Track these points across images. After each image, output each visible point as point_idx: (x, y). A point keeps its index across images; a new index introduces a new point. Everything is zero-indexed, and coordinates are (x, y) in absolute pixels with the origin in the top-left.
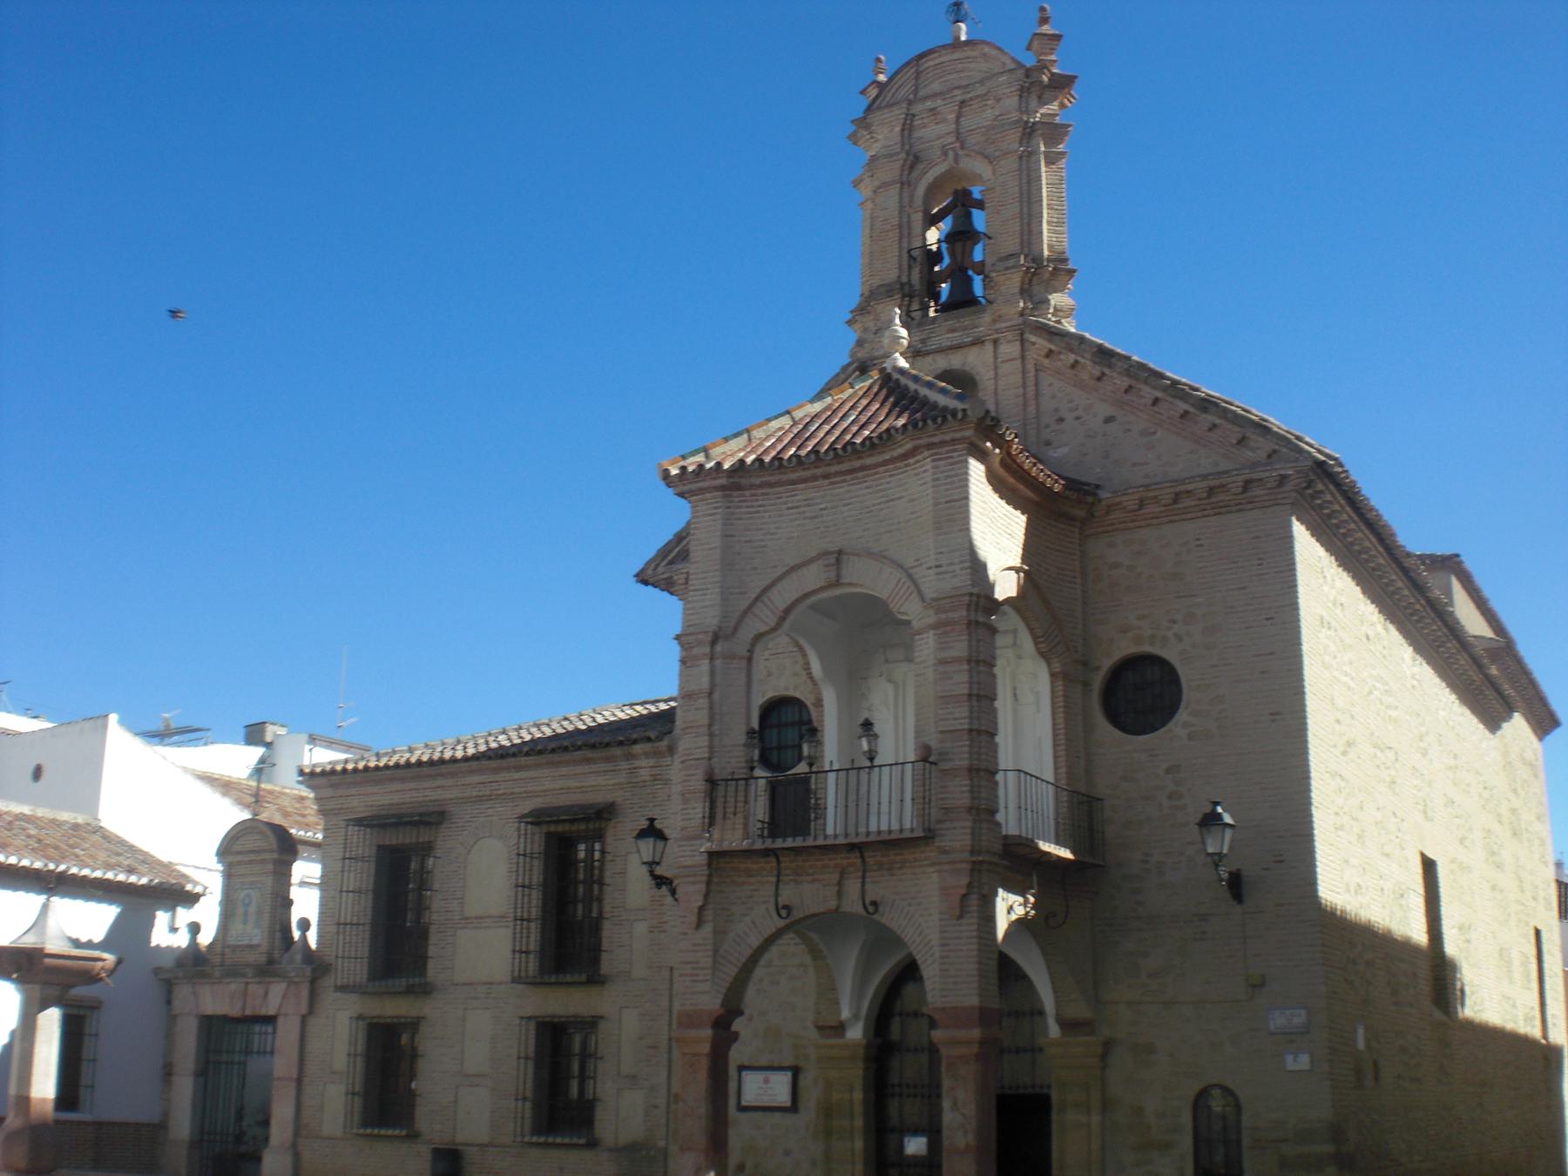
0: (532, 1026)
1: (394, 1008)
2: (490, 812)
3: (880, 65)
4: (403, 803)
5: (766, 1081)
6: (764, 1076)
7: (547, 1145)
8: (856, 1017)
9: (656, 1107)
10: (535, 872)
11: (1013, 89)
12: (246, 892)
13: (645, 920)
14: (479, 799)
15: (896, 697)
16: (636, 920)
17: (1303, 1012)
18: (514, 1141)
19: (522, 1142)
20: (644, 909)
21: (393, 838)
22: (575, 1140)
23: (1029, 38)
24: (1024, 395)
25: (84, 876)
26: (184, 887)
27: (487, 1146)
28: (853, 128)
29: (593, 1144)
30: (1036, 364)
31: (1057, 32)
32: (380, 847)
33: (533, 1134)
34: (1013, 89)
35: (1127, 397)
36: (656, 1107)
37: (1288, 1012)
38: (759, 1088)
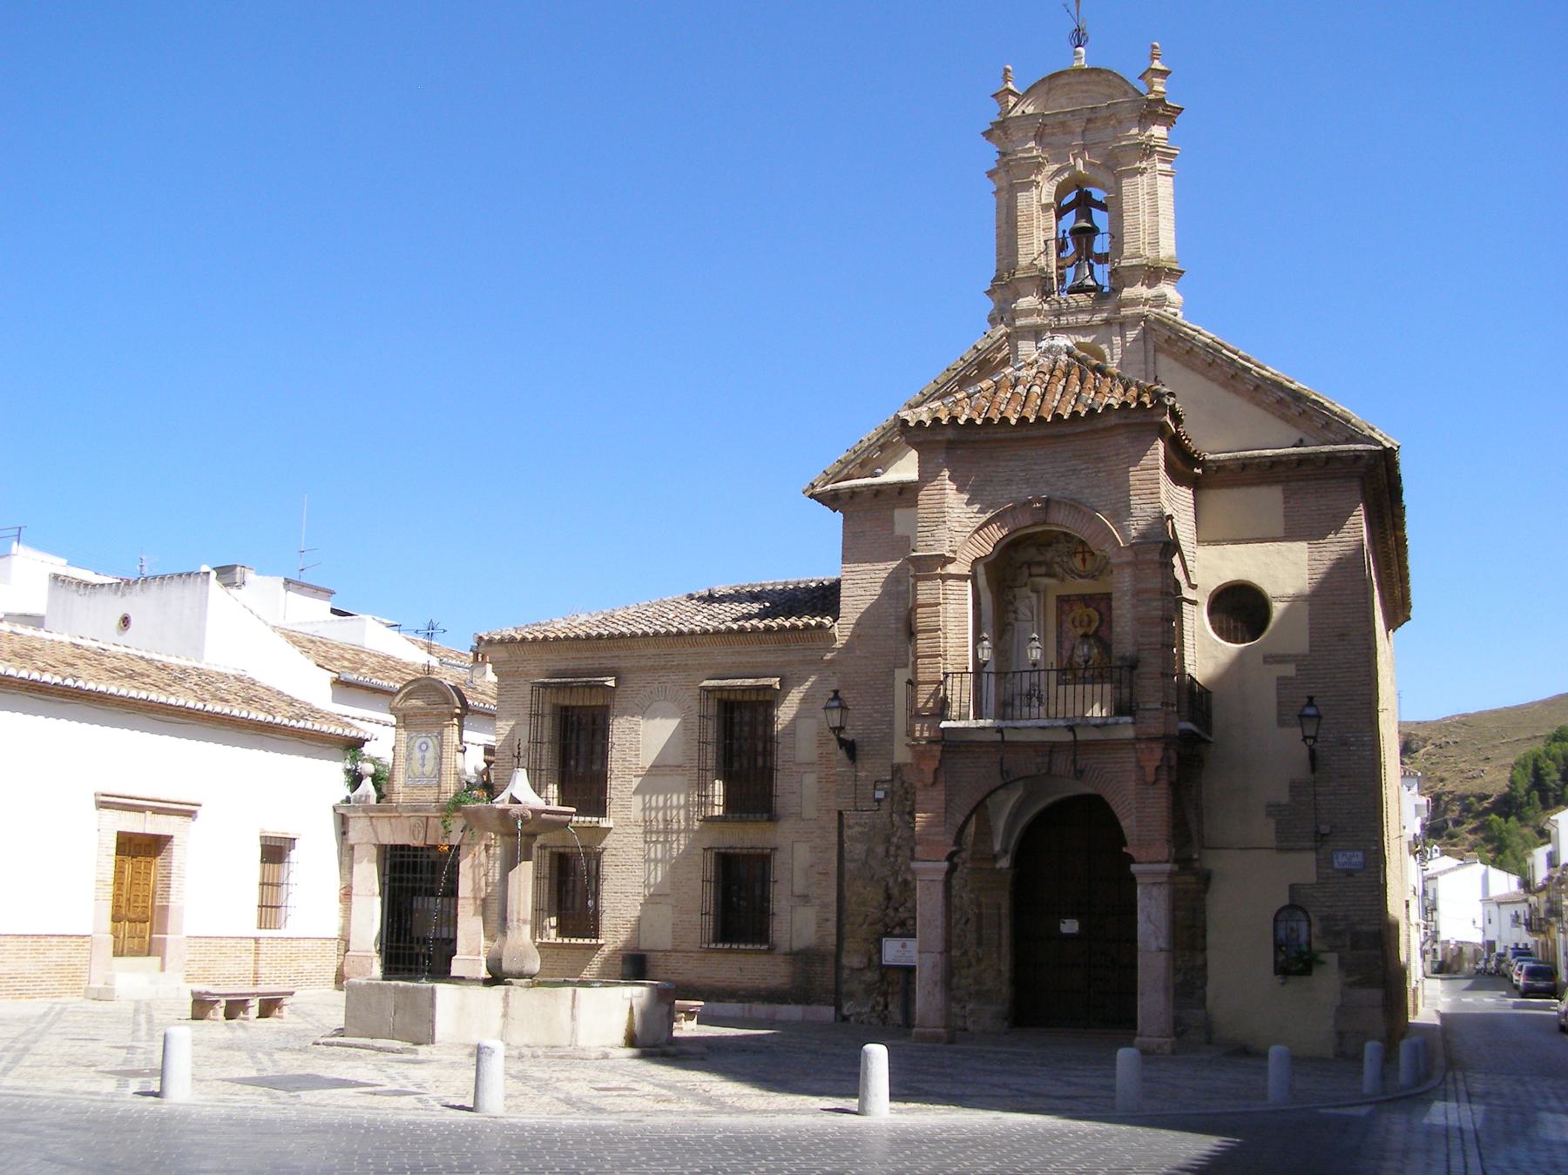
0: (711, 856)
1: (746, 837)
2: (663, 679)
3: (1009, 74)
4: (579, 669)
5: (904, 946)
6: (901, 942)
7: (730, 951)
8: (1005, 851)
9: (827, 920)
10: (710, 731)
11: (1135, 115)
12: (424, 739)
13: (814, 772)
14: (653, 669)
15: (1039, 602)
16: (805, 772)
17: (1360, 854)
18: (701, 947)
19: (708, 948)
20: (813, 764)
21: (566, 700)
22: (757, 946)
23: (1145, 70)
24: (1146, 369)
25: (292, 726)
26: (1180, 868)
27: (670, 951)
28: (990, 127)
29: (771, 950)
30: (1155, 346)
31: (1166, 69)
32: (555, 706)
33: (715, 941)
34: (1135, 115)
35: (1232, 382)
36: (827, 920)
37: (1348, 854)
38: (898, 951)
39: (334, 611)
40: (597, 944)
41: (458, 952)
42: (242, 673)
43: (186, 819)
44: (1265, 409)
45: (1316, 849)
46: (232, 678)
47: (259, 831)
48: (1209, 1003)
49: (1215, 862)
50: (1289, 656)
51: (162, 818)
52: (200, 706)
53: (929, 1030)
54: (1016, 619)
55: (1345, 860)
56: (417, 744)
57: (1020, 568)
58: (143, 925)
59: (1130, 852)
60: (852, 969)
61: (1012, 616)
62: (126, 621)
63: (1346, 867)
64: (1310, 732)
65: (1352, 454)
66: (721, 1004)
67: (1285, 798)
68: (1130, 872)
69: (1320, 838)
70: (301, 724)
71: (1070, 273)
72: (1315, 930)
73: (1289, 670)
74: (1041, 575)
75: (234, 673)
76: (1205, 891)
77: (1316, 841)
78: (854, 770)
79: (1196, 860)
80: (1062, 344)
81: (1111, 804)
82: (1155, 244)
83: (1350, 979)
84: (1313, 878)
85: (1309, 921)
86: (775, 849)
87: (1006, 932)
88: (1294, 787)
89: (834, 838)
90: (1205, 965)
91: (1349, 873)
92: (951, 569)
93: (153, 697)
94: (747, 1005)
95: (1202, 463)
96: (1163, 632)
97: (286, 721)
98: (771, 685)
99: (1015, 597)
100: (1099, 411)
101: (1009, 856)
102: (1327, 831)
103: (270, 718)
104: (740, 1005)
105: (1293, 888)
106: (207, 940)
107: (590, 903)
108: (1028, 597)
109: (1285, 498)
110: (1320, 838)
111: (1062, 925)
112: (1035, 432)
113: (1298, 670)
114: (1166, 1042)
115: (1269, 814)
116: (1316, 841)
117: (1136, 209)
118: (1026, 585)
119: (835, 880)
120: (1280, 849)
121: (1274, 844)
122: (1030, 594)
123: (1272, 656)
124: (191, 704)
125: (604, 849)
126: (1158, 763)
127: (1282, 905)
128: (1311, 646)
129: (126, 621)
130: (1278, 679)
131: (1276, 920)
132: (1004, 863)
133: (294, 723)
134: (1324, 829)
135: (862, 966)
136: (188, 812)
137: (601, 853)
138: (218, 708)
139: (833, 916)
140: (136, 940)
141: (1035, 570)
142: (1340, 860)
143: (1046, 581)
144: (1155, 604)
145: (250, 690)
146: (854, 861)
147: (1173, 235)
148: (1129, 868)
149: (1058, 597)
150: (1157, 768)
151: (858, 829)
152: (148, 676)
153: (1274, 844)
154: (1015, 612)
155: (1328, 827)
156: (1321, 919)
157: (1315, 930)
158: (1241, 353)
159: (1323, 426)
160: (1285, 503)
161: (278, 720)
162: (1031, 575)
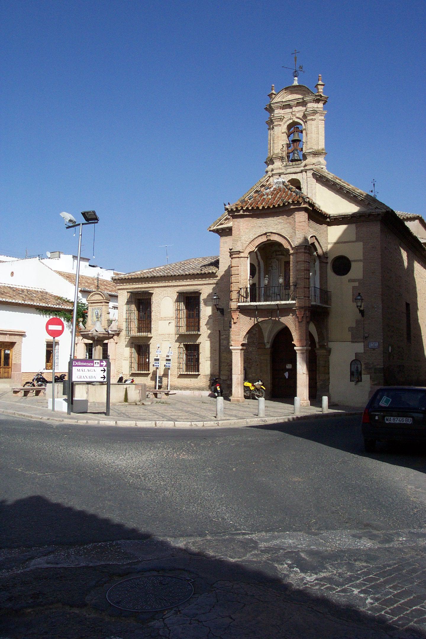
25: (55, 307)
35: (340, 190)
39: (90, 266)
40: (148, 373)
41: (119, 378)
42: (44, 290)
43: (20, 337)
44: (350, 199)
45: (364, 342)
46: (39, 292)
47: (45, 340)
48: (330, 391)
49: (331, 345)
50: (356, 279)
51: (13, 337)
52: (23, 302)
53: (236, 398)
54: (272, 269)
55: (372, 345)
56: (95, 312)
57: (273, 252)
58: (8, 369)
59: (294, 343)
60: (224, 380)
61: (270, 268)
62: (12, 273)
63: (373, 347)
64: (359, 304)
65: (376, 213)
66: (185, 391)
67: (354, 325)
68: (294, 350)
69: (366, 338)
70: (58, 306)
71: (291, 155)
72: (363, 367)
73: (356, 284)
74: (279, 255)
75: (41, 290)
76: (329, 355)
77: (364, 339)
78: (223, 318)
79: (326, 345)
80: (281, 181)
81: (290, 328)
82: (318, 144)
83: (374, 383)
84: (362, 351)
85: (361, 365)
86: (200, 343)
87: (269, 368)
88: (357, 322)
89: (218, 339)
90: (329, 379)
91: (374, 349)
92: (242, 255)
93: (7, 300)
94: (192, 391)
95: (329, 217)
96: (305, 274)
97: (52, 306)
98: (198, 292)
99: (271, 262)
100: (266, 208)
101: (269, 344)
102: (367, 336)
103: (47, 305)
104: (190, 391)
105: (356, 354)
106: (29, 373)
107: (147, 360)
108: (276, 262)
109: (356, 228)
110: (366, 338)
111: (287, 366)
112: (273, 211)
113: (359, 284)
114: (305, 402)
115: (349, 331)
116: (364, 339)
117: (311, 133)
118: (275, 258)
119: (218, 352)
120: (352, 342)
121: (351, 340)
122: (277, 261)
123: (351, 279)
124: (20, 302)
125: (150, 343)
126: (302, 315)
127: (353, 359)
128: (363, 276)
129: (12, 273)
130: (353, 287)
131: (351, 364)
132: (268, 346)
133: (55, 306)
134: (366, 335)
135: (226, 379)
136: (22, 335)
137: (149, 345)
138: (29, 303)
139: (218, 363)
140: (6, 374)
141: (278, 253)
142: (371, 345)
143: (280, 256)
144: (302, 265)
145: (43, 295)
146: (224, 346)
147: (324, 141)
148: (294, 348)
149: (285, 262)
150: (302, 317)
151: (225, 336)
152: (9, 293)
153: (351, 340)
154: (272, 267)
155: (367, 334)
156: (365, 364)
157: (363, 367)
158: (342, 180)
159: (368, 204)
160: (356, 229)
161: (50, 305)
162: (276, 255)
